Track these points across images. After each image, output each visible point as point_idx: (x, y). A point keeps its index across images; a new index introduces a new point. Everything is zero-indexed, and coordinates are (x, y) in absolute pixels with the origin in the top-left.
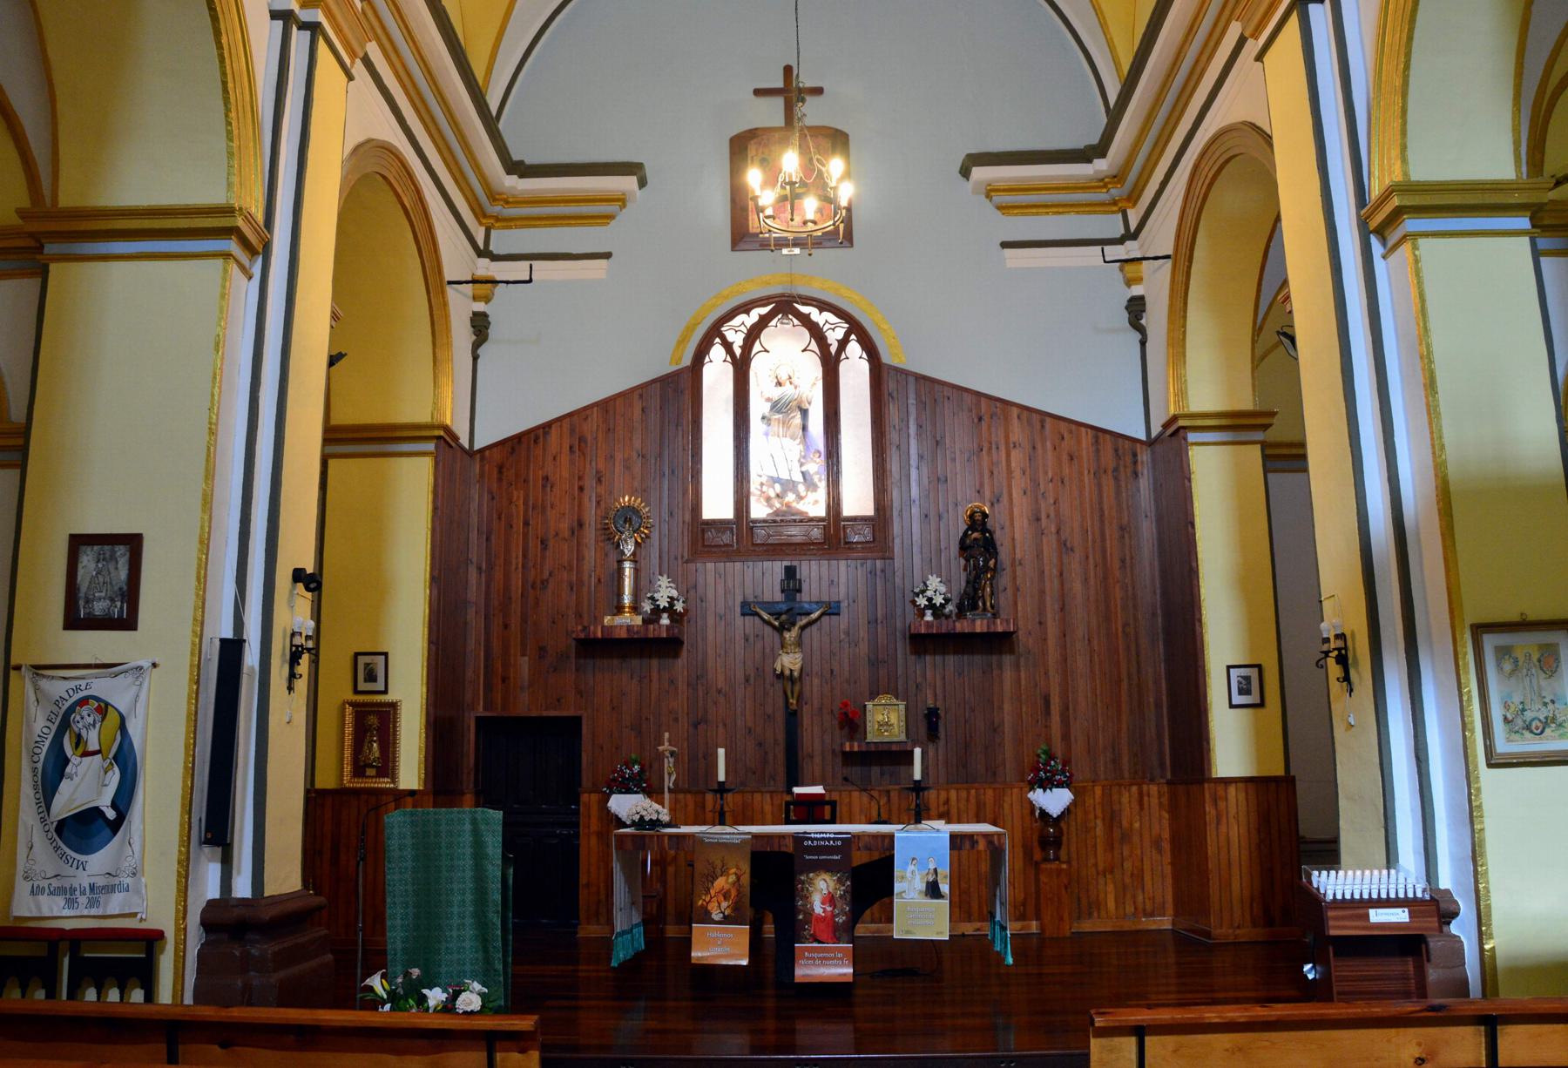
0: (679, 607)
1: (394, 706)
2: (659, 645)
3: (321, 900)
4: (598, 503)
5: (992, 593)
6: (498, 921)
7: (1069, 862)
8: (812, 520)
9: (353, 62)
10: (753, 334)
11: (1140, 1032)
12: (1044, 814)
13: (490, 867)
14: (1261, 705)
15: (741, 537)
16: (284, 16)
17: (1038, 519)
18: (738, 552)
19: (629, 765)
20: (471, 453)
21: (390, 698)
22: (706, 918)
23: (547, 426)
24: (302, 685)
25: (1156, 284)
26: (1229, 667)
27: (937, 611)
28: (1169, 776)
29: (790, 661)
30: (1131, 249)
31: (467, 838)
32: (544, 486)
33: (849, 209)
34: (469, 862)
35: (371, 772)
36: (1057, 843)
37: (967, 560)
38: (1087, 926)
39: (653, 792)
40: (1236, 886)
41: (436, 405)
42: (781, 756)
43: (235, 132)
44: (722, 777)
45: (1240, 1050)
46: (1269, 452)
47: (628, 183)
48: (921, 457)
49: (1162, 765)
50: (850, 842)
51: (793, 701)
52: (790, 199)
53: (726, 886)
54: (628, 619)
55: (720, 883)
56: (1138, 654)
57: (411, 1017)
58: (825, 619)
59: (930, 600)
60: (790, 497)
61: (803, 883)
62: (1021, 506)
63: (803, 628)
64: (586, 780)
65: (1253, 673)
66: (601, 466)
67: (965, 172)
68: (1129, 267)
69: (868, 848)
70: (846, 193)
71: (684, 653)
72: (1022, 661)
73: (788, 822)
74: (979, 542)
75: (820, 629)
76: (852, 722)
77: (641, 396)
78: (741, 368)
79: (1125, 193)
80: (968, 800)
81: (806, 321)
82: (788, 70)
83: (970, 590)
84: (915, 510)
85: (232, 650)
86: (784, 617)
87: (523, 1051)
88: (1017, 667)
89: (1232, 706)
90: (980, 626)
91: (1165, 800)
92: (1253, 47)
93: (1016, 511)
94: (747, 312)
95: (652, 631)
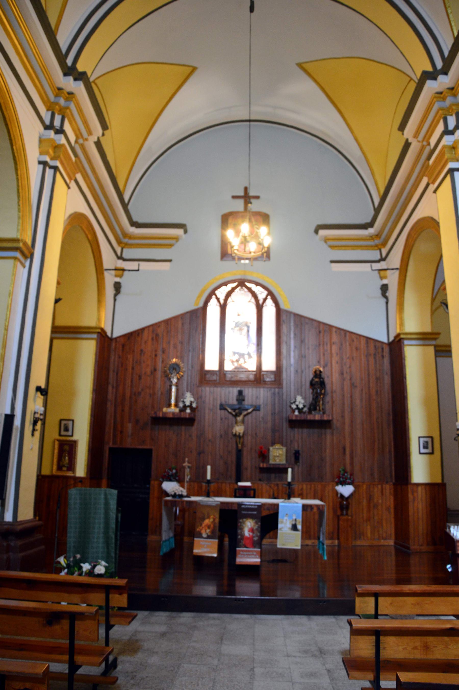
0: (194, 405)
1: (75, 442)
2: (185, 421)
3: (41, 523)
4: (163, 361)
5: (323, 404)
6: (113, 536)
7: (352, 516)
8: (250, 371)
9: (70, 182)
10: (229, 295)
11: (376, 595)
12: (342, 496)
13: (111, 514)
14: (432, 453)
15: (221, 378)
16: (44, 164)
17: (342, 374)
18: (219, 383)
19: (171, 469)
20: (111, 339)
21: (74, 438)
22: (200, 536)
23: (143, 330)
24: (37, 434)
25: (392, 280)
26: (419, 438)
27: (300, 410)
28: (394, 481)
29: (239, 429)
30: (382, 265)
31: (102, 501)
32: (141, 354)
33: (268, 248)
34: (102, 511)
35: (65, 469)
36: (347, 508)
37: (313, 390)
38: (359, 543)
39: (180, 481)
40: (421, 528)
41: (99, 320)
42: (234, 468)
43: (21, 209)
44: (209, 477)
45: (418, 604)
46: (437, 349)
47: (180, 232)
48: (295, 347)
49: (391, 476)
50: (261, 507)
51: (240, 446)
52: (245, 241)
53: (209, 523)
54: (173, 409)
55: (207, 522)
56: (382, 431)
57: (75, 577)
58: (254, 412)
59: (297, 406)
60: (242, 361)
61: (241, 523)
62: (336, 368)
63: (245, 416)
64: (153, 473)
65: (429, 440)
66: (165, 346)
67: (316, 232)
68: (382, 272)
69: (268, 509)
70: (267, 241)
71: (196, 424)
72: (335, 432)
73: (235, 496)
74: (318, 383)
75: (252, 416)
76: (264, 455)
77: (182, 319)
78: (223, 308)
79: (381, 242)
80: (310, 489)
81: (250, 290)
82: (246, 189)
83: (314, 402)
84: (292, 369)
85: (9, 419)
86: (237, 411)
87: (120, 594)
88: (332, 434)
89: (420, 453)
90: (317, 417)
91: (392, 491)
92: (432, 187)
93: (334, 370)
94: (226, 285)
95: (183, 415)
